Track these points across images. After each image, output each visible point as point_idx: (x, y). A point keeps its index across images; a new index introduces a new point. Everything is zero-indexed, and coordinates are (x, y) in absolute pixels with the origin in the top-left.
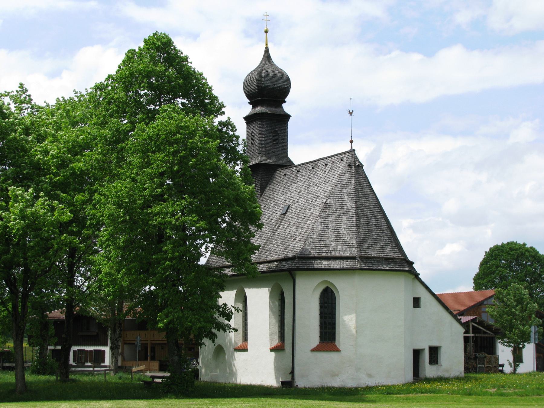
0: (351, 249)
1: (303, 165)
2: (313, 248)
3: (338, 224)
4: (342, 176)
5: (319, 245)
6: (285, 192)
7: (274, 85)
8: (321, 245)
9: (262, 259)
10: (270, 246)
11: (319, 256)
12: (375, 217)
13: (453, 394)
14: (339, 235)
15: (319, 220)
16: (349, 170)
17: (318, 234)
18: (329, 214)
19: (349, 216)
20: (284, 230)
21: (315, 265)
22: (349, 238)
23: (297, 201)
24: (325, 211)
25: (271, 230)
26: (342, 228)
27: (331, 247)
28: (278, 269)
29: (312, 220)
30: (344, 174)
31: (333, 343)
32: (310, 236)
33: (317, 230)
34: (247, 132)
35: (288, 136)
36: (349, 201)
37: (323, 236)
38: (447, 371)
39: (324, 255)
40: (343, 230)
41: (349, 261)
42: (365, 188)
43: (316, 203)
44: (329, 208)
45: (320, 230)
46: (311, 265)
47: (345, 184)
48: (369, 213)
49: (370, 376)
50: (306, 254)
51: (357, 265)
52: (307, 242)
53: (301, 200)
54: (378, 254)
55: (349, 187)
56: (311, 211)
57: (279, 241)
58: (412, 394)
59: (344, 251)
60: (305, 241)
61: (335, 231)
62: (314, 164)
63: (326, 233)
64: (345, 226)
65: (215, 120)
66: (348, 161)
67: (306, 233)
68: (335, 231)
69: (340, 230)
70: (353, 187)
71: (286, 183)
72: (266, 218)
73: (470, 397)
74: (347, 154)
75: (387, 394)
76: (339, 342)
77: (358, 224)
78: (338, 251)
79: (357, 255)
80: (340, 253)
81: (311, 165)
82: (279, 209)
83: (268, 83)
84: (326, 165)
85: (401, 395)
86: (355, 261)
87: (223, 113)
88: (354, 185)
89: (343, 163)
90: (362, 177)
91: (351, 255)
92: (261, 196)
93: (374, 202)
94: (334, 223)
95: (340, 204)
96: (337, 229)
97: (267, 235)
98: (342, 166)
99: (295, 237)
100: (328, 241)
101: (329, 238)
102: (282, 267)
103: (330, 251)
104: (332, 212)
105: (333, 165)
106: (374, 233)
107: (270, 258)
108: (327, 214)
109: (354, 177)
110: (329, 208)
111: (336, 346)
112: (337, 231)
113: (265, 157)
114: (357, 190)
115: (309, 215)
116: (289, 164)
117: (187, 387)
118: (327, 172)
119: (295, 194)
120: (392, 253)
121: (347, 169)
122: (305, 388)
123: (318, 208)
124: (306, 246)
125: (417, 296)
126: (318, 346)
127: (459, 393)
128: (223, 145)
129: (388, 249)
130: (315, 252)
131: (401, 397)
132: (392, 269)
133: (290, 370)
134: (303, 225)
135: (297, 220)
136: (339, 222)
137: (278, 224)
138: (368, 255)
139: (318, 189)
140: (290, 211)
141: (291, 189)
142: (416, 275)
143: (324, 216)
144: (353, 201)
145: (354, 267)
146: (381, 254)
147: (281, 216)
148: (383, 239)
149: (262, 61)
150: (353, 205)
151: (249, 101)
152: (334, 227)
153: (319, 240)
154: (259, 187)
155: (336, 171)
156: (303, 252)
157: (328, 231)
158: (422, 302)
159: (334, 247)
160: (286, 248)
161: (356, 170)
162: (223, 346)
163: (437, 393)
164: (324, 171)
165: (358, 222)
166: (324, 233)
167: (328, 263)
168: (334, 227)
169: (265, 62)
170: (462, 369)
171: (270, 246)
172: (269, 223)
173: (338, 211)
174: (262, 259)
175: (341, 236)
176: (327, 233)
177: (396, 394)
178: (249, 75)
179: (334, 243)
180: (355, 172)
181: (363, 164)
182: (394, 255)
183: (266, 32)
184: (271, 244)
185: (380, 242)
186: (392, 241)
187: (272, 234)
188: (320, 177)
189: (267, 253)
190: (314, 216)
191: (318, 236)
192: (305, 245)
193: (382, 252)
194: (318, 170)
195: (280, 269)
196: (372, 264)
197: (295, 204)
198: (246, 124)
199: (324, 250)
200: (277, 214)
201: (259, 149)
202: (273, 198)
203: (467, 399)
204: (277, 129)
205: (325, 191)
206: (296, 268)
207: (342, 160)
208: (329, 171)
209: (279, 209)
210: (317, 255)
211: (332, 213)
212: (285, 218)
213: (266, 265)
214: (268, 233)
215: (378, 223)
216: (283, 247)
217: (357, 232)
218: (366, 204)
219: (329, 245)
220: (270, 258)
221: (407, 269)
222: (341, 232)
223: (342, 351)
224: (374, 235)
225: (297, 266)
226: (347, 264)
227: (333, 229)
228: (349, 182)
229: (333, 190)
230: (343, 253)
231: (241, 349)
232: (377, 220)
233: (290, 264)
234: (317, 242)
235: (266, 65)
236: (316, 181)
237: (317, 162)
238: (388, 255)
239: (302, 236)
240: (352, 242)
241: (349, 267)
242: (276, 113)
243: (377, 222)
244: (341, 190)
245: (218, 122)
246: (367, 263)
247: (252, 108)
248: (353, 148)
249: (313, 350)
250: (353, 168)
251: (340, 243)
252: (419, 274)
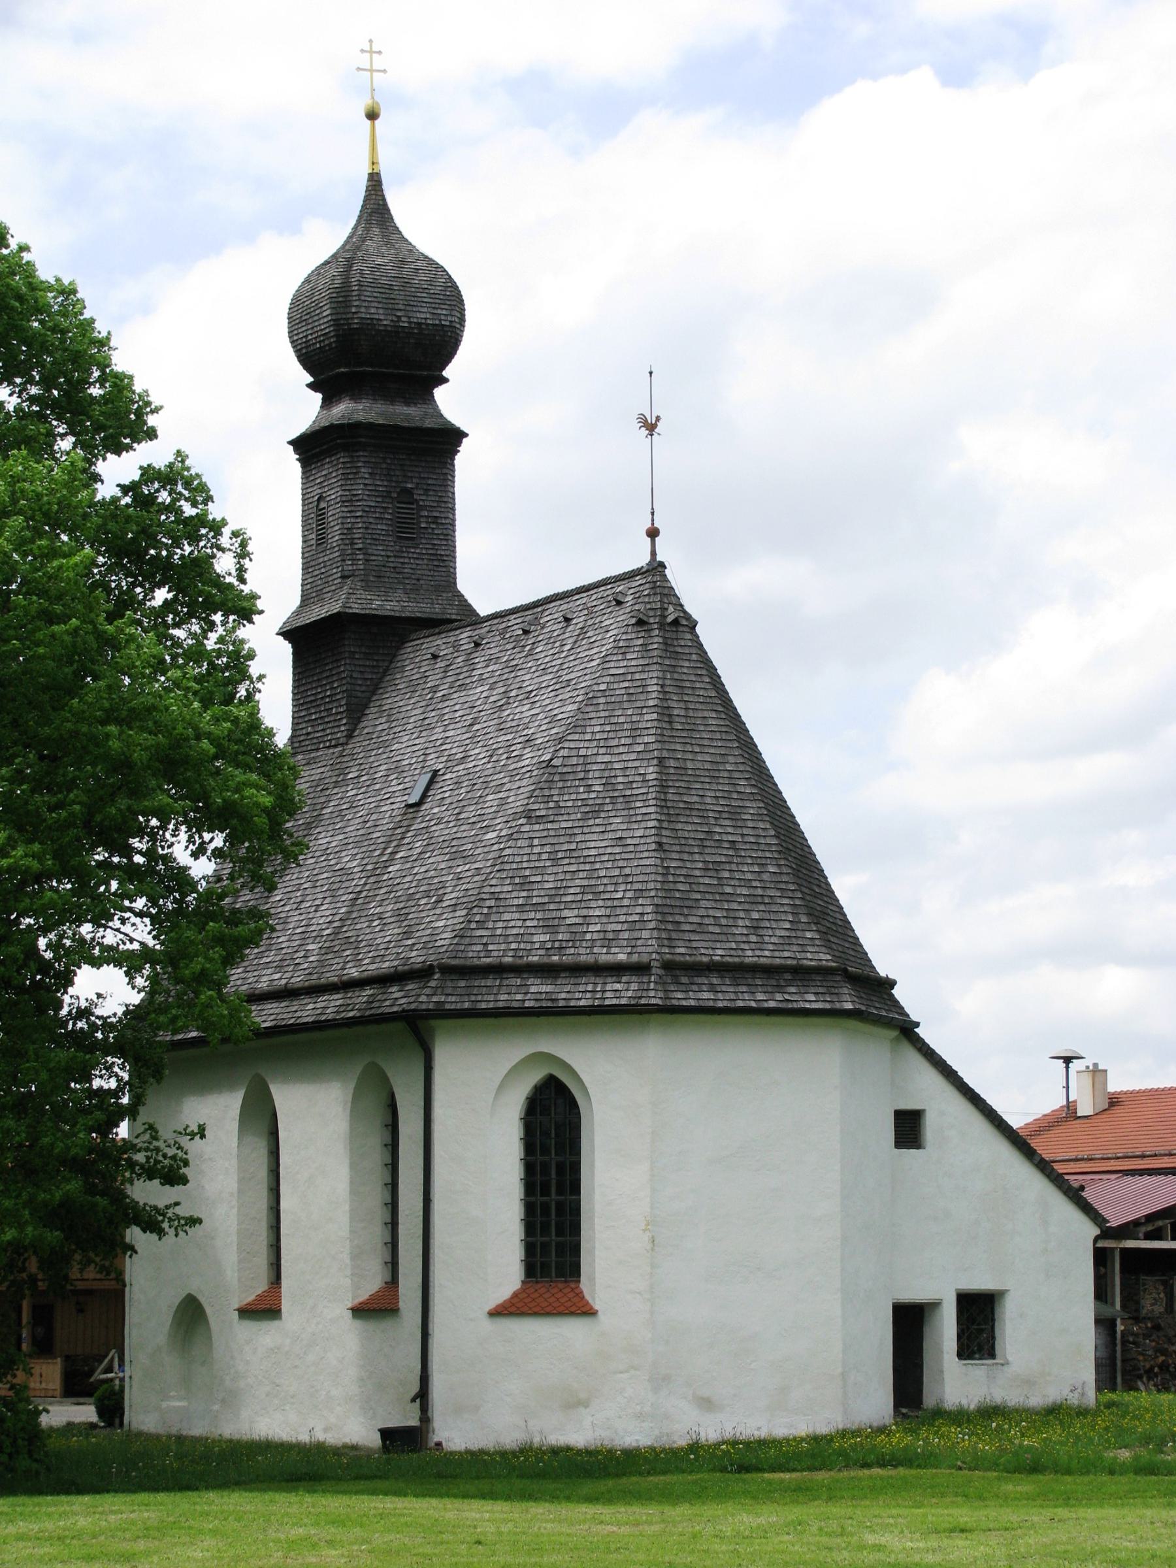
0: (636, 934)
1: (496, 621)
2: (499, 932)
3: (595, 843)
4: (612, 664)
5: (520, 923)
6: (427, 722)
7: (399, 317)
8: (528, 923)
9: (328, 975)
10: (358, 926)
11: (519, 961)
12: (735, 815)
13: (975, 1469)
14: (593, 882)
15: (523, 829)
16: (640, 642)
17: (517, 880)
18: (561, 804)
19: (632, 812)
20: (409, 865)
21: (502, 997)
22: (629, 894)
23: (461, 755)
24: (546, 792)
25: (369, 867)
26: (606, 858)
27: (562, 929)
28: (372, 1012)
29: (501, 830)
30: (620, 657)
31: (573, 1285)
32: (486, 890)
33: (514, 866)
34: (303, 495)
35: (453, 509)
36: (634, 756)
37: (535, 886)
38: (1029, 1382)
39: (536, 959)
40: (609, 865)
41: (624, 979)
42: (698, 706)
43: (520, 764)
44: (560, 785)
45: (525, 865)
46: (485, 998)
47: (623, 691)
48: (708, 800)
49: (706, 1404)
50: (470, 955)
51: (652, 994)
52: (475, 911)
53: (477, 751)
54: (740, 953)
55: (639, 704)
56: (501, 795)
57: (390, 908)
58: (830, 1470)
59: (608, 942)
60: (472, 909)
61: (582, 867)
62: (529, 616)
63: (546, 878)
64: (617, 850)
65: (101, 467)
66: (637, 607)
67: (476, 879)
68: (582, 867)
69: (597, 866)
70: (651, 703)
71: (434, 689)
72: (357, 821)
73: (1034, 1477)
74: (639, 580)
75: (739, 1472)
76: (592, 1279)
77: (664, 840)
78: (589, 944)
79: (654, 956)
80: (596, 950)
81: (519, 620)
82: (401, 787)
83: (373, 311)
84: (567, 620)
85: (787, 1476)
86: (645, 979)
87: (152, 434)
88: (654, 695)
89: (622, 612)
90: (687, 664)
91: (635, 958)
92: (350, 736)
93: (731, 759)
94: (579, 838)
95: (603, 766)
96: (588, 860)
97: (354, 883)
98: (616, 623)
99: (441, 892)
100: (552, 907)
101: (556, 894)
102: (387, 1003)
103: (557, 945)
104: (573, 797)
105: (590, 622)
106: (727, 875)
107: (354, 973)
108: (551, 805)
109: (655, 667)
110: (560, 785)
111: (580, 1295)
112: (588, 867)
113: (367, 588)
114: (665, 714)
115: (493, 809)
116: (467, 616)
117: (10, 1455)
118: (567, 647)
119: (459, 732)
120: (795, 948)
121: (633, 636)
122: (468, 1452)
123: (525, 782)
124: (473, 925)
125: (909, 1104)
126: (515, 1295)
127: (998, 1465)
128: (159, 554)
129: (778, 933)
130: (503, 947)
131: (782, 1481)
132: (790, 1006)
133: (415, 1388)
134: (470, 846)
135: (455, 830)
136: (595, 837)
137: (394, 844)
138: (699, 958)
139: (533, 712)
140: (436, 794)
141: (447, 710)
142: (907, 1030)
143: (543, 813)
144: (649, 756)
145: (643, 1001)
146: (749, 953)
147: (405, 814)
148: (762, 896)
149: (355, 228)
150: (651, 769)
151: (310, 379)
152: (575, 854)
153: (521, 901)
154: (343, 702)
155: (597, 644)
156: (462, 948)
157: (555, 870)
158: (931, 1127)
159: (573, 929)
160: (407, 934)
161: (664, 638)
162: (202, 1300)
163: (919, 1466)
164: (558, 644)
165: (664, 833)
166: (539, 878)
167: (549, 988)
168: (575, 854)
169: (367, 229)
170: (1087, 1374)
171: (358, 926)
172: (364, 838)
173: (593, 795)
174: (328, 975)
175: (601, 888)
176: (551, 878)
177: (773, 1470)
178: (307, 281)
179: (576, 912)
180: (662, 646)
181: (695, 616)
182: (803, 955)
183: (372, 115)
184: (363, 920)
185: (747, 907)
186: (798, 902)
187: (372, 880)
188: (542, 667)
189: (348, 953)
190: (510, 812)
191: (518, 888)
192: (470, 922)
193: (753, 946)
194: (540, 638)
195: (380, 1011)
196: (712, 988)
197: (456, 769)
198: (298, 464)
199: (536, 938)
200: (394, 806)
201: (344, 560)
202: (385, 745)
203: (1024, 1486)
204: (410, 486)
205: (553, 720)
206: (431, 1006)
207: (619, 603)
208: (576, 642)
209: (401, 787)
210: (510, 959)
211: (570, 804)
212: (419, 820)
213: (336, 997)
214: (358, 875)
215: (742, 835)
216: (400, 931)
217: (660, 870)
218: (699, 765)
219: (556, 922)
220: (354, 970)
221: (849, 1006)
222: (602, 873)
223: (599, 1313)
224: (725, 882)
225: (435, 999)
226: (619, 991)
227: (573, 861)
228: (639, 683)
229: (580, 716)
230: (605, 950)
231: (380, 1310)
232: (740, 823)
233: (414, 993)
234: (514, 909)
235: (368, 243)
236: (529, 680)
237: (540, 609)
238: (777, 954)
239: (464, 887)
240: (639, 910)
241: (624, 1001)
242: (406, 424)
243: (739, 831)
244: (607, 714)
245: (141, 468)
246: (695, 988)
247: (322, 407)
248: (659, 558)
249: (498, 1312)
250: (657, 632)
251: (597, 913)
252: (917, 1025)
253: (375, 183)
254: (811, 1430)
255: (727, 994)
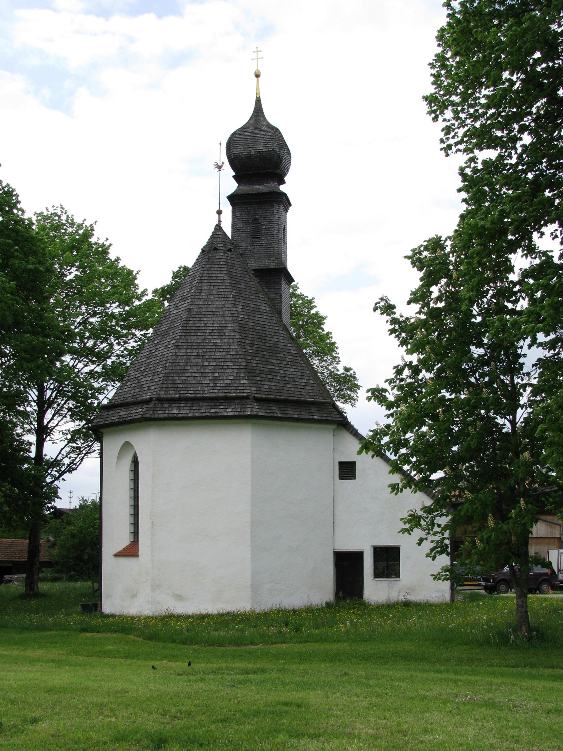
12: (220, 332)
183: (257, 76)
196: (179, 408)
253: (258, 101)
254: (206, 612)
255: (186, 410)
